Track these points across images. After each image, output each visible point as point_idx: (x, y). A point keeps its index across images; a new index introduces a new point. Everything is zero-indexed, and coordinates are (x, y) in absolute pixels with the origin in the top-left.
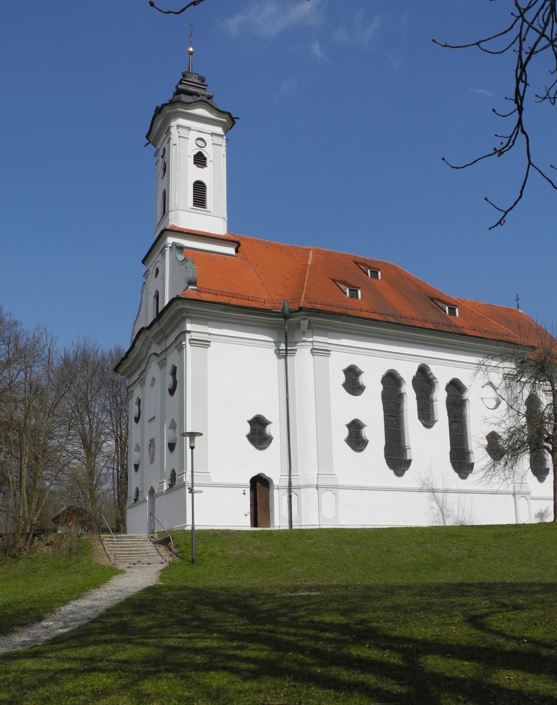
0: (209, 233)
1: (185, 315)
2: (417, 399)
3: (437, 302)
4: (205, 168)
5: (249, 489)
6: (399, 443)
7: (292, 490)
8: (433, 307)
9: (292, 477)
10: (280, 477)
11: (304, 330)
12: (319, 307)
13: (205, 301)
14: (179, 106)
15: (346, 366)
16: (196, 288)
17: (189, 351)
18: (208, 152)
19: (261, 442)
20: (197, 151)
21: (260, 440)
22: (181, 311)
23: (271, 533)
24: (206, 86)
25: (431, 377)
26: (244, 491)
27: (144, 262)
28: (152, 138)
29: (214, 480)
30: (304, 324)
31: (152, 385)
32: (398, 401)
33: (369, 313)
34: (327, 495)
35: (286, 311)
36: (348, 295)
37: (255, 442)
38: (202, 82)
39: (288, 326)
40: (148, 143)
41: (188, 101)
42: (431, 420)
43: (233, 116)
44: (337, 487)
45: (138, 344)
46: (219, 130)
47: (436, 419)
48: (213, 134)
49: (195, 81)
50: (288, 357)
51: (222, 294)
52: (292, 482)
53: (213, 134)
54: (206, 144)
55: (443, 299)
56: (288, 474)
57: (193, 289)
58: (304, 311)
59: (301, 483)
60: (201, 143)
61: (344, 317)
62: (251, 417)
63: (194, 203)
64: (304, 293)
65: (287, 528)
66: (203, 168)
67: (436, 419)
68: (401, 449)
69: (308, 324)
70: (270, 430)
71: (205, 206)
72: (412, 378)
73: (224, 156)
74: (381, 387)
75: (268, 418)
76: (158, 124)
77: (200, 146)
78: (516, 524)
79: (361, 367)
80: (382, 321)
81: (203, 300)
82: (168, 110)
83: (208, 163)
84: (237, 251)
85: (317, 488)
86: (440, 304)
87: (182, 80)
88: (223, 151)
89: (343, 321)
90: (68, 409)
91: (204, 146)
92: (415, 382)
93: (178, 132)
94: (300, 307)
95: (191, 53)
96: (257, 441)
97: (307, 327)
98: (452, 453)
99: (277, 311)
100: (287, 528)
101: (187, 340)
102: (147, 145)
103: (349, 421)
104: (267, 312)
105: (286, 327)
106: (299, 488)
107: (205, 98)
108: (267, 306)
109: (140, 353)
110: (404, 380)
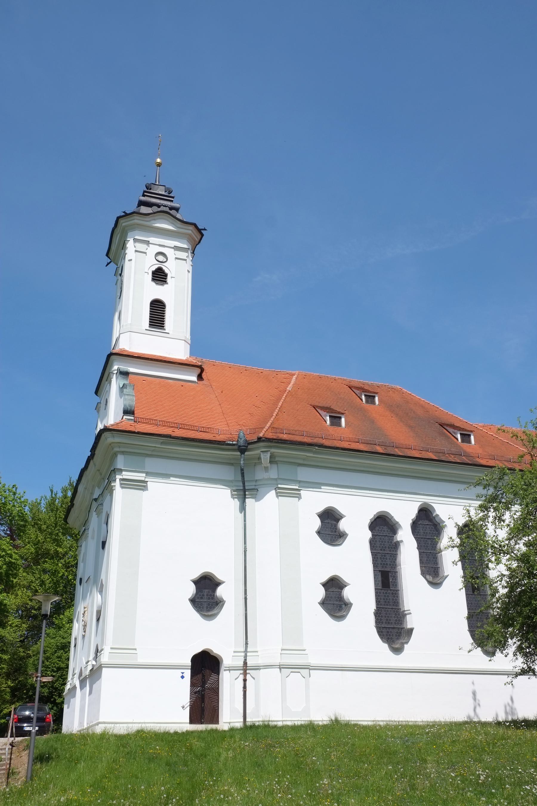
0: (165, 357)
1: (116, 449)
2: (419, 548)
3: (447, 428)
4: (166, 286)
5: (189, 671)
6: (397, 606)
7: (248, 671)
8: (444, 434)
9: (248, 654)
10: (280, 651)
11: (265, 465)
12: (285, 437)
13: (138, 433)
14: (135, 217)
15: (321, 509)
16: (133, 418)
17: (119, 493)
18: (170, 268)
19: (211, 608)
20: (156, 267)
21: (209, 605)
23: (216, 730)
24: (173, 197)
26: (183, 673)
27: (96, 393)
29: (141, 660)
32: (393, 551)
33: (350, 443)
35: (242, 442)
36: (328, 422)
37: (203, 608)
38: (169, 194)
39: (244, 460)
40: (111, 262)
42: (441, 575)
43: (200, 227)
47: (446, 574)
48: (176, 248)
49: (160, 193)
50: (247, 499)
51: (165, 424)
52: (247, 661)
53: (176, 248)
54: (167, 259)
55: (458, 425)
58: (263, 441)
59: (260, 661)
60: (161, 258)
61: (317, 448)
62: (325, 579)
63: (150, 324)
64: (270, 421)
66: (162, 285)
67: (446, 574)
68: (399, 615)
69: (271, 457)
71: (163, 327)
72: (411, 521)
73: (189, 271)
74: (369, 535)
75: (219, 575)
77: (161, 260)
78: (468, 724)
79: (341, 510)
80: (366, 452)
81: (136, 431)
82: (123, 223)
83: (169, 279)
85: (280, 668)
86: (451, 430)
87: (145, 192)
88: (187, 266)
89: (314, 453)
91: (165, 260)
92: (415, 526)
93: (135, 247)
94: (259, 437)
95: (159, 165)
96: (205, 606)
97: (269, 462)
98: (377, 614)
99: (231, 443)
101: (118, 480)
102: (108, 264)
104: (218, 444)
105: (242, 462)
106: (257, 668)
107: (167, 209)
108: (219, 438)
110: (400, 526)
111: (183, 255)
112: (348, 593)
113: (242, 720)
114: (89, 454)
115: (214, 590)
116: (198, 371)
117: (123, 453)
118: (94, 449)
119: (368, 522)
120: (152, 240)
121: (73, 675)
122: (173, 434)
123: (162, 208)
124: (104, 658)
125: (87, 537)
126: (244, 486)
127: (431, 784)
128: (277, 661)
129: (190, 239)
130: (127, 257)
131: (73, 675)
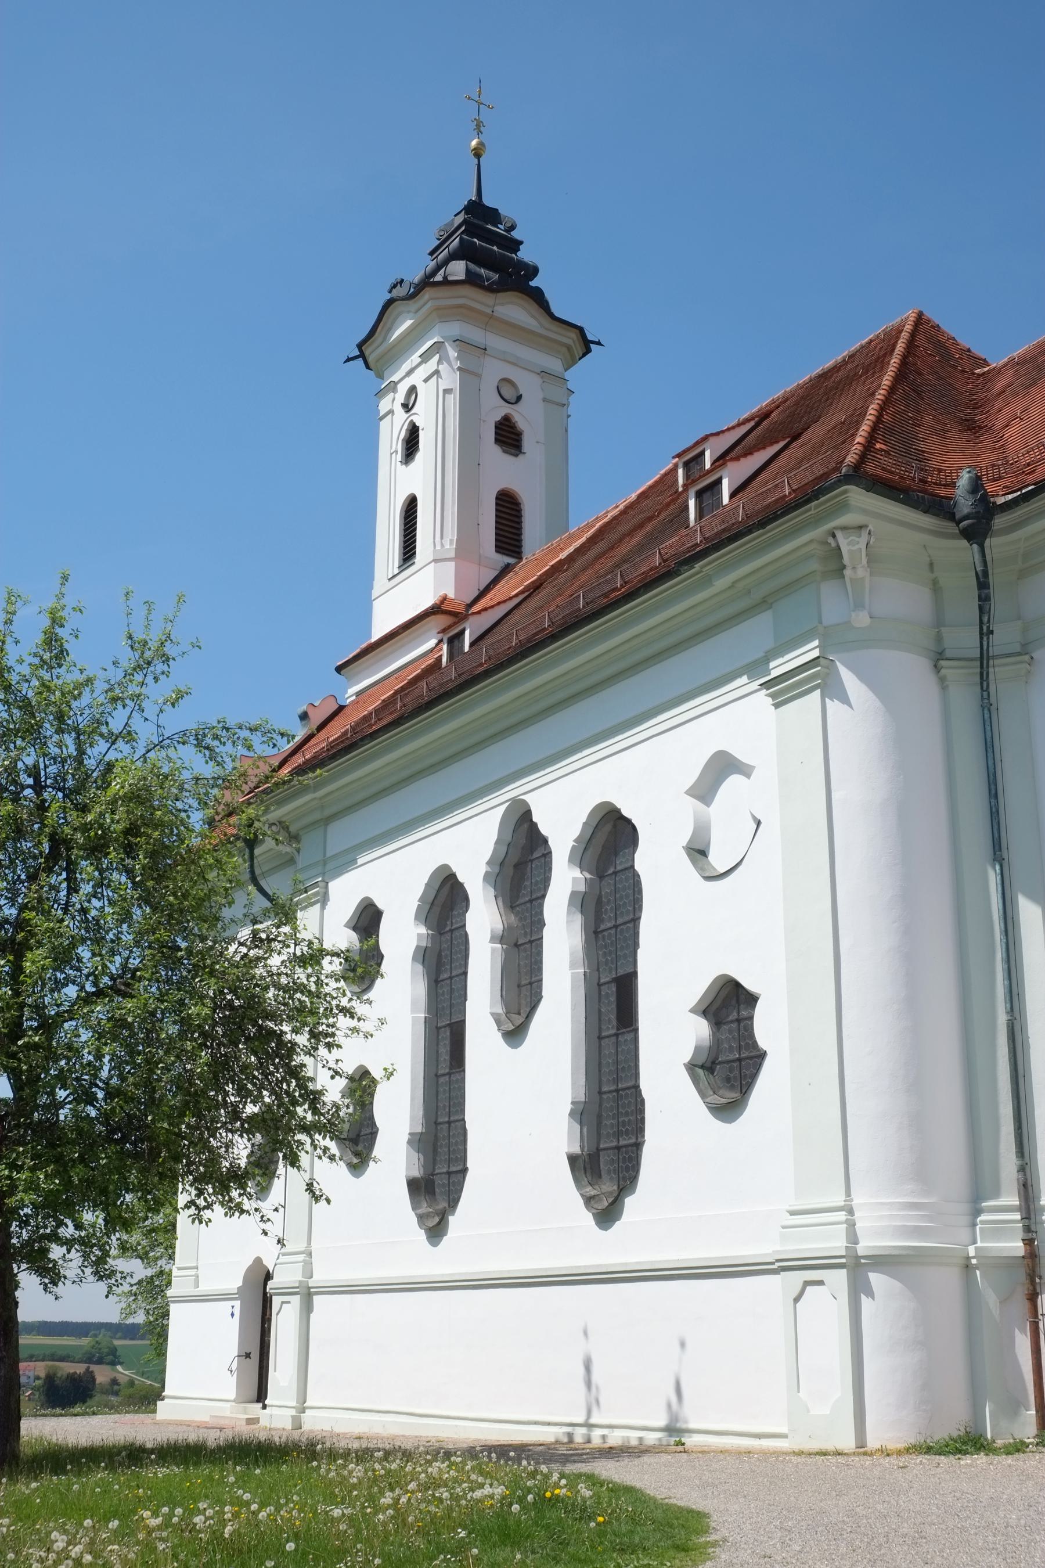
53: (425, 357)
111: (432, 364)
120: (395, 378)
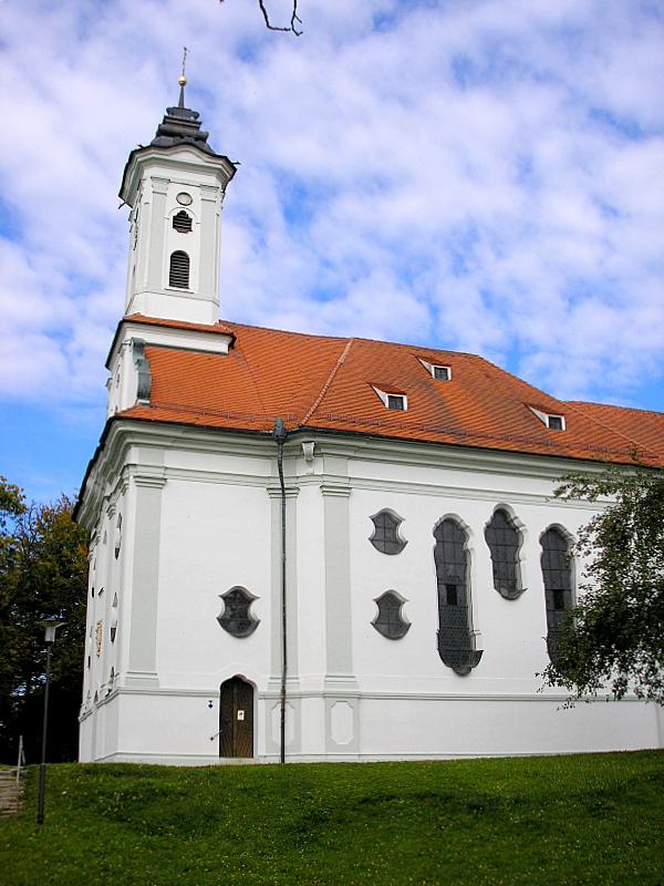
1: (129, 440)
5: (219, 700)
10: (324, 678)
22: (123, 434)
24: (200, 123)
25: (516, 522)
28: (126, 195)
29: (164, 686)
30: (308, 448)
31: (105, 542)
34: (342, 710)
36: (387, 405)
41: (166, 144)
44: (360, 697)
45: (90, 483)
46: (213, 180)
51: (188, 409)
56: (280, 676)
57: (144, 404)
59: (302, 689)
60: (184, 199)
62: (225, 590)
65: (277, 760)
70: (255, 610)
75: (252, 590)
76: (131, 178)
84: (231, 346)
90: (585, 634)
92: (490, 530)
98: (440, 635)
100: (277, 760)
103: (379, 594)
109: (92, 497)
111: (211, 195)
112: (406, 612)
113: (280, 754)
114: (98, 444)
115: (248, 607)
116: (230, 339)
117: (137, 444)
118: (103, 439)
119: (432, 527)
121: (89, 698)
122: (198, 423)
123: (186, 139)
124: (121, 683)
125: (97, 542)
126: (282, 485)
127: (156, 795)
128: (321, 689)
129: (220, 174)
130: (144, 200)
131: (89, 698)
